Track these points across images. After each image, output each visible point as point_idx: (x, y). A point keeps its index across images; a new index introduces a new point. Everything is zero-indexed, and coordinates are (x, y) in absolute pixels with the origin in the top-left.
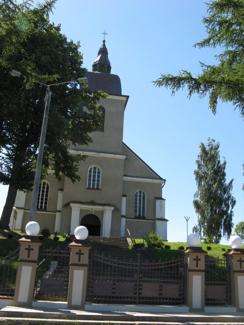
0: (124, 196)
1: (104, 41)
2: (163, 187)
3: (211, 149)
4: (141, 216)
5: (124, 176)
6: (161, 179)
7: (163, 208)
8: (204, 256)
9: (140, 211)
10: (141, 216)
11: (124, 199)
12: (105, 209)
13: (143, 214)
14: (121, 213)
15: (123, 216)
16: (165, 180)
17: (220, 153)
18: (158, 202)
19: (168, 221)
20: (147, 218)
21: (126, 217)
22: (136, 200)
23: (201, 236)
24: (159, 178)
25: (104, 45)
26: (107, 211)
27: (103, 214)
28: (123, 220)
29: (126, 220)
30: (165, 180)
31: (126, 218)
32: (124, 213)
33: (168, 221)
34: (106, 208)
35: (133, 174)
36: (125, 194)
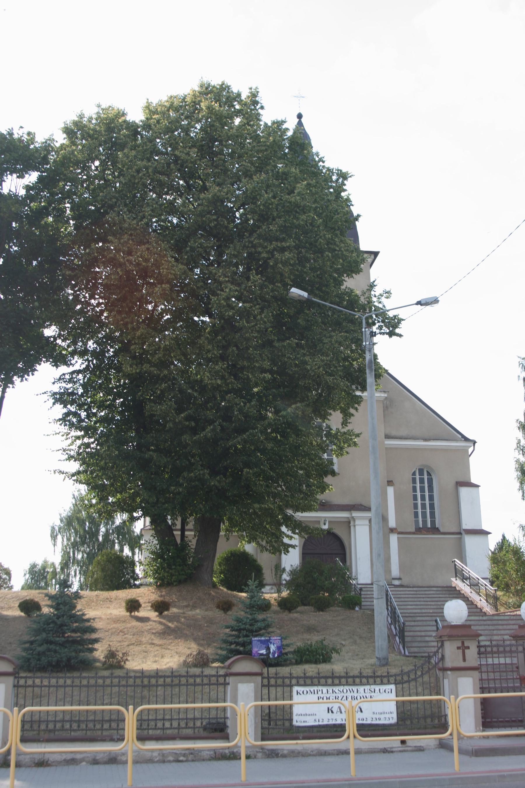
0: (390, 483)
1: (300, 116)
2: (470, 455)
3: (269, 135)
4: (429, 525)
5: (388, 437)
6: (466, 439)
7: (476, 504)
8: (395, 703)
9: (424, 515)
10: (429, 525)
11: (390, 491)
12: (353, 517)
13: (433, 522)
14: (388, 522)
15: (392, 530)
16: (474, 442)
17: (349, 185)
18: (464, 491)
19: (490, 533)
20: (442, 530)
21: (399, 530)
22: (414, 489)
23: (468, 585)
24: (460, 436)
25: (300, 124)
26: (357, 522)
27: (350, 527)
28: (394, 539)
29: (398, 538)
30: (474, 442)
31: (399, 533)
32: (392, 523)
33: (490, 533)
34: (355, 514)
35: (403, 432)
36: (391, 480)
